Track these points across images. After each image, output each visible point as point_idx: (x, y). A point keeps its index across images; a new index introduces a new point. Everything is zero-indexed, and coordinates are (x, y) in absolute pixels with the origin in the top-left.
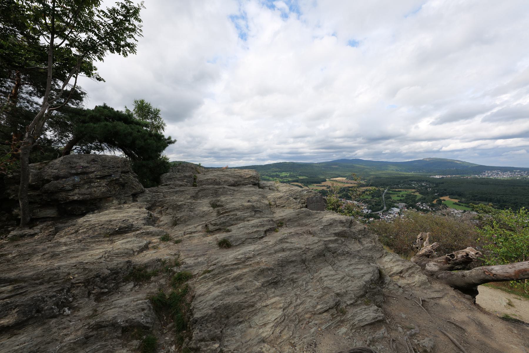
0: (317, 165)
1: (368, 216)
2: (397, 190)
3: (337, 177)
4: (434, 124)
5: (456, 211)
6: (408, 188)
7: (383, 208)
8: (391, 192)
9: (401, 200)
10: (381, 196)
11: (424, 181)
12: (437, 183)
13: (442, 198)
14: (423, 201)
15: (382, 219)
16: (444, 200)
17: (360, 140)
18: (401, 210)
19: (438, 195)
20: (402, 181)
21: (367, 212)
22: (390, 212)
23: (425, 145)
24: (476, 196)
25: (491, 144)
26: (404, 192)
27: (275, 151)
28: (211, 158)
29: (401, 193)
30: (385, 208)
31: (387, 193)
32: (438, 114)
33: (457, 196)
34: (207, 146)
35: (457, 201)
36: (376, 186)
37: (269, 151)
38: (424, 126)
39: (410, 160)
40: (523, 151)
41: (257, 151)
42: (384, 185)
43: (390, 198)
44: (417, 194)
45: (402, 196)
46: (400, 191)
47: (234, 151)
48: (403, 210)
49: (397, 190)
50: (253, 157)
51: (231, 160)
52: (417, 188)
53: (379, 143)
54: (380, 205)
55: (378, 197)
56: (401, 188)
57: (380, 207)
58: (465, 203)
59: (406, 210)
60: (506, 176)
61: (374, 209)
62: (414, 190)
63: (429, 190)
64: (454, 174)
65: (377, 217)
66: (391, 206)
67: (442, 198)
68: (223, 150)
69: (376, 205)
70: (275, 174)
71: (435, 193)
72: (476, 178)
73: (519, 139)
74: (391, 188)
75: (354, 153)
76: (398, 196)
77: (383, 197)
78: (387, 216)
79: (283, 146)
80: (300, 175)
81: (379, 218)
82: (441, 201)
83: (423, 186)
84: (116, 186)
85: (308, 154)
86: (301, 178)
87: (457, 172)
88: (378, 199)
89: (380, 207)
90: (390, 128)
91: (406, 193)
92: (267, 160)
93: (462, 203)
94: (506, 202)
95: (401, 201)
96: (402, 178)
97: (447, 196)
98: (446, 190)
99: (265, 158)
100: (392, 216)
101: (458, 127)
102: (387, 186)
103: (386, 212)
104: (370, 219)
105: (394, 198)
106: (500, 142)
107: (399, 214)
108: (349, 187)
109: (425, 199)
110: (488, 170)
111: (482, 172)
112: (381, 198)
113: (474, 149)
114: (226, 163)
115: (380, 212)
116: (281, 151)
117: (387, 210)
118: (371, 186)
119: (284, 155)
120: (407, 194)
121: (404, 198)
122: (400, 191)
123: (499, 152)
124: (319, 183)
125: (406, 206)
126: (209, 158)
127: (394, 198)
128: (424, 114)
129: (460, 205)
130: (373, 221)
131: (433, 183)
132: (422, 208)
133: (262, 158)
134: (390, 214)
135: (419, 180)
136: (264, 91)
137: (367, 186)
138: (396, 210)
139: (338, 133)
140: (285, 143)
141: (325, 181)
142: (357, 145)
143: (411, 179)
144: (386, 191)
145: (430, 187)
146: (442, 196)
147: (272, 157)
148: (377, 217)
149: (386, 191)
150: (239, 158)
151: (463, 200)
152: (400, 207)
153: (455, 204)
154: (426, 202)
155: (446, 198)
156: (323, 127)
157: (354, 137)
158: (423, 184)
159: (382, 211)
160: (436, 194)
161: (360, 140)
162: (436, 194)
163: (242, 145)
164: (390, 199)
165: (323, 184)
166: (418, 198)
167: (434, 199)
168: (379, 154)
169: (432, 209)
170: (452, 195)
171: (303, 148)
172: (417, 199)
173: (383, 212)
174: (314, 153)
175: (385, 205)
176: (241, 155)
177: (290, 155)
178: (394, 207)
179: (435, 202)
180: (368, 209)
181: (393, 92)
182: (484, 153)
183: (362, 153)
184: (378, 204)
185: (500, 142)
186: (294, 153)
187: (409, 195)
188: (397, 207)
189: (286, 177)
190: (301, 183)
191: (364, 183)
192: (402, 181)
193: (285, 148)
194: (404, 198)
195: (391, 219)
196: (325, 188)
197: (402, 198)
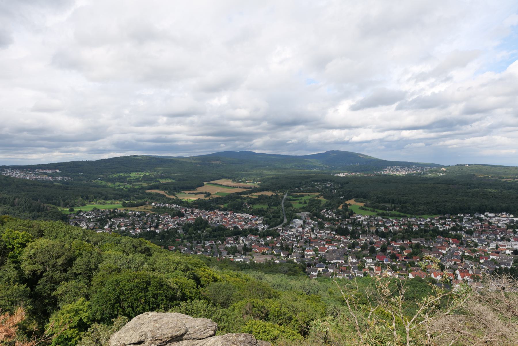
0: (189, 161)
1: (264, 235)
2: (298, 194)
4: (354, 108)
5: (362, 218)
6: (311, 191)
7: (282, 221)
8: (291, 197)
9: (303, 208)
10: (280, 204)
11: (327, 181)
12: (343, 182)
13: (347, 202)
14: (329, 207)
15: (282, 236)
16: (350, 205)
17: (265, 124)
18: (304, 222)
19: (344, 198)
20: (304, 182)
21: (263, 229)
22: (291, 225)
23: (336, 134)
24: (380, 197)
25: (396, 136)
26: (307, 197)
27: (128, 137)
30: (285, 220)
31: (287, 200)
32: (360, 98)
33: (362, 199)
35: (362, 204)
36: (273, 191)
37: (117, 137)
38: (342, 111)
39: (313, 153)
40: (421, 144)
41: (94, 135)
42: (282, 188)
43: (291, 206)
44: (321, 198)
45: (305, 203)
47: (48, 135)
48: (307, 221)
49: (298, 194)
50: (83, 146)
51: (35, 152)
53: (288, 130)
55: (276, 205)
56: (303, 192)
57: (279, 220)
58: (371, 207)
59: (310, 221)
60: (402, 173)
61: (272, 224)
62: (317, 194)
63: (334, 192)
64: (357, 172)
65: (275, 235)
66: (292, 217)
67: (347, 202)
68: (21, 130)
69: (274, 217)
72: (378, 175)
73: (421, 131)
74: (292, 192)
76: (300, 203)
77: (283, 206)
78: (288, 232)
79: (146, 128)
80: (162, 177)
81: (278, 235)
82: (346, 205)
83: (327, 188)
84: (495, 295)
85: (184, 143)
86: (163, 181)
88: (275, 208)
89: (279, 220)
90: (310, 108)
91: (309, 197)
92: (110, 151)
93: (367, 206)
94: (405, 202)
95: (304, 209)
96: (304, 178)
97: (352, 199)
98: (350, 191)
99: (109, 147)
100: (294, 231)
101: (376, 114)
102: (287, 189)
103: (286, 227)
104: (268, 239)
105: (296, 205)
106: (406, 134)
107: (303, 227)
108: (237, 193)
109: (330, 204)
111: (384, 168)
113: (381, 141)
114: (21, 156)
115: (279, 227)
117: (288, 224)
120: (310, 200)
121: (307, 205)
122: (302, 196)
123: (402, 144)
124: (193, 188)
125: (309, 216)
127: (296, 205)
128: (346, 95)
129: (365, 210)
131: (338, 183)
132: (327, 216)
133: (101, 148)
134: (292, 228)
137: (262, 190)
138: (299, 222)
139: (243, 112)
140: (151, 123)
141: (203, 185)
142: (259, 131)
143: (313, 179)
144: (285, 196)
145: (335, 189)
146: (347, 200)
147: (121, 145)
148: (275, 235)
149: (285, 196)
150: (52, 148)
152: (303, 217)
153: (361, 208)
155: (352, 202)
156: (219, 102)
157: (256, 121)
158: (327, 185)
159: (281, 225)
161: (265, 124)
163: (68, 124)
164: (290, 208)
165: (200, 189)
166: (323, 203)
167: (339, 203)
168: (283, 144)
169: (338, 217)
170: (358, 197)
172: (321, 206)
173: (283, 226)
174: (194, 141)
175: (285, 217)
176: (60, 141)
177: (154, 144)
178: (295, 218)
180: (264, 224)
183: (259, 145)
184: (277, 215)
185: (406, 134)
186: (161, 141)
187: (312, 201)
188: (300, 218)
189: (137, 180)
190: (163, 189)
191: (258, 186)
192: (304, 182)
193: (149, 132)
194: (307, 205)
196: (202, 197)
197: (305, 205)
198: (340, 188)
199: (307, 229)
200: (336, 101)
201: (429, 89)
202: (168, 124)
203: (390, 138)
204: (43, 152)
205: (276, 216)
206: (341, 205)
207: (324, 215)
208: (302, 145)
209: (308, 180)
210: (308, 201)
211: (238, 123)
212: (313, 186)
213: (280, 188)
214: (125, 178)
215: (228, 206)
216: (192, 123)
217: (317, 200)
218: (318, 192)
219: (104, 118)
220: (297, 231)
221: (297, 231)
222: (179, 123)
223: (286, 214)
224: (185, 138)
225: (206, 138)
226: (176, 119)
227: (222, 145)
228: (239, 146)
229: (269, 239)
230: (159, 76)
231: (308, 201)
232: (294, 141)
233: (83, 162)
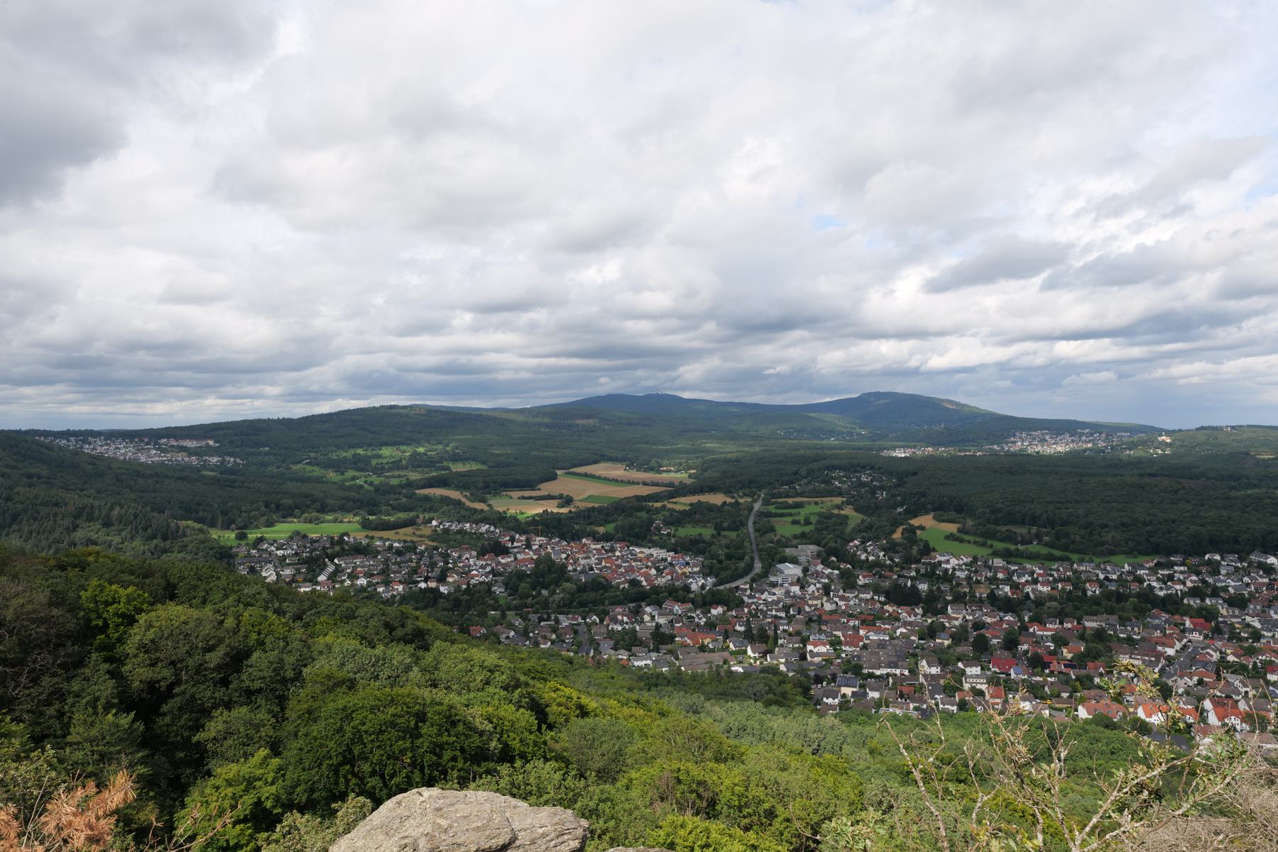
1: (705, 602)
2: (790, 501)
3: (581, 465)
4: (935, 287)
5: (954, 562)
7: (750, 567)
8: (772, 509)
9: (803, 535)
11: (864, 468)
12: (903, 472)
13: (915, 522)
14: (868, 533)
15: (749, 606)
16: (922, 528)
17: (710, 327)
18: (805, 570)
20: (803, 471)
21: (703, 587)
22: (772, 579)
23: (887, 350)
24: (999, 510)
25: (1040, 354)
26: (812, 509)
27: (380, 361)
28: (60, 387)
29: (803, 512)
30: (758, 567)
31: (762, 514)
32: (950, 260)
33: (952, 514)
34: (58, 327)
35: (952, 528)
36: (727, 492)
37: (352, 361)
38: (904, 295)
41: (298, 357)
43: (772, 530)
44: (848, 511)
45: (808, 522)
46: (799, 505)
47: (196, 358)
48: (812, 569)
49: (790, 501)
50: (273, 383)
52: (848, 493)
53: (765, 341)
54: (741, 558)
55: (736, 529)
56: (802, 494)
57: (742, 565)
58: (975, 534)
59: (820, 567)
61: (724, 575)
62: (838, 500)
63: (882, 496)
65: (731, 601)
66: (773, 558)
67: (915, 522)
68: (133, 346)
69: (729, 557)
70: (349, 454)
71: (895, 506)
72: (995, 454)
73: (1106, 341)
74: (774, 496)
75: (674, 374)
76: (794, 522)
81: (741, 604)
83: (864, 485)
85: (527, 375)
86: (458, 468)
87: (948, 438)
88: (733, 535)
89: (742, 565)
90: (825, 288)
91: (817, 509)
92: (334, 395)
93: (967, 533)
95: (804, 538)
97: (927, 513)
98: (923, 495)
99: (332, 387)
100: (779, 592)
101: (991, 301)
102: (760, 488)
103: (761, 582)
104: (714, 612)
105: (785, 528)
106: (1066, 349)
109: (869, 528)
110: (1022, 430)
112: (743, 530)
113: (1003, 367)
115: (743, 584)
116: (405, 360)
117: (765, 575)
118: (712, 490)
119: (410, 376)
120: (819, 514)
122: (799, 505)
124: (531, 485)
125: (819, 555)
126: (49, 389)
127: (785, 528)
128: (916, 254)
129: (962, 541)
130: (722, 618)
131: (891, 473)
132: (863, 557)
133: (315, 388)
134: (774, 585)
135: (853, 467)
136: (425, 119)
137: (700, 490)
138: (792, 570)
139: (658, 300)
141: (553, 477)
142: (696, 344)
143: (827, 462)
144: (757, 506)
145: (882, 488)
146: (915, 516)
147: (361, 381)
148: (731, 601)
149: (757, 506)
150: (203, 388)
151: (970, 523)
152: (802, 559)
153: (950, 537)
154: (876, 539)
155: (926, 520)
156: (601, 274)
157: (689, 320)
158: (864, 478)
159: (748, 579)
160: (900, 510)
162: (900, 510)
163: (240, 330)
164: (771, 535)
165: (546, 488)
166: (852, 525)
167: (895, 524)
168: (753, 376)
170: (942, 510)
171: (500, 350)
173: (753, 580)
174: (537, 370)
175: (756, 556)
176: (224, 372)
178: (783, 560)
179: (897, 536)
180: (705, 576)
181: (853, 176)
182: (1022, 377)
183: (694, 380)
184: (736, 552)
185: (1066, 349)
187: (825, 517)
188: (794, 561)
189: (397, 465)
190: (457, 488)
191: (689, 482)
192: (803, 471)
193: (428, 349)
195: (777, 603)
196: (552, 507)
197: (807, 529)
198: (897, 486)
199: (812, 588)
200: (888, 270)
201: (1128, 237)
202: (475, 329)
203: (1025, 361)
204: (181, 398)
205: (734, 556)
206: (900, 529)
207: (855, 555)
208: (800, 378)
209: (814, 466)
210: (814, 519)
211: (645, 326)
212: (827, 481)
213: (744, 487)
214: (367, 460)
215: (616, 529)
216: (533, 327)
217: (839, 516)
218: (840, 495)
219: (327, 318)
220: (788, 592)
221: (788, 592)
222: (499, 327)
223: (760, 550)
224: (514, 362)
225: (552, 361)
226: (495, 318)
227: (603, 380)
228: (643, 381)
229: (717, 611)
230: (460, 215)
231: (814, 519)
232: (781, 368)
233: (269, 422)
